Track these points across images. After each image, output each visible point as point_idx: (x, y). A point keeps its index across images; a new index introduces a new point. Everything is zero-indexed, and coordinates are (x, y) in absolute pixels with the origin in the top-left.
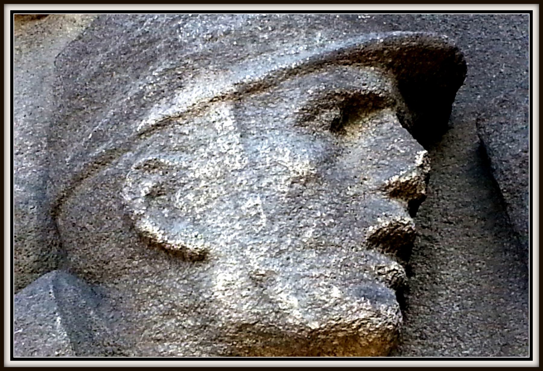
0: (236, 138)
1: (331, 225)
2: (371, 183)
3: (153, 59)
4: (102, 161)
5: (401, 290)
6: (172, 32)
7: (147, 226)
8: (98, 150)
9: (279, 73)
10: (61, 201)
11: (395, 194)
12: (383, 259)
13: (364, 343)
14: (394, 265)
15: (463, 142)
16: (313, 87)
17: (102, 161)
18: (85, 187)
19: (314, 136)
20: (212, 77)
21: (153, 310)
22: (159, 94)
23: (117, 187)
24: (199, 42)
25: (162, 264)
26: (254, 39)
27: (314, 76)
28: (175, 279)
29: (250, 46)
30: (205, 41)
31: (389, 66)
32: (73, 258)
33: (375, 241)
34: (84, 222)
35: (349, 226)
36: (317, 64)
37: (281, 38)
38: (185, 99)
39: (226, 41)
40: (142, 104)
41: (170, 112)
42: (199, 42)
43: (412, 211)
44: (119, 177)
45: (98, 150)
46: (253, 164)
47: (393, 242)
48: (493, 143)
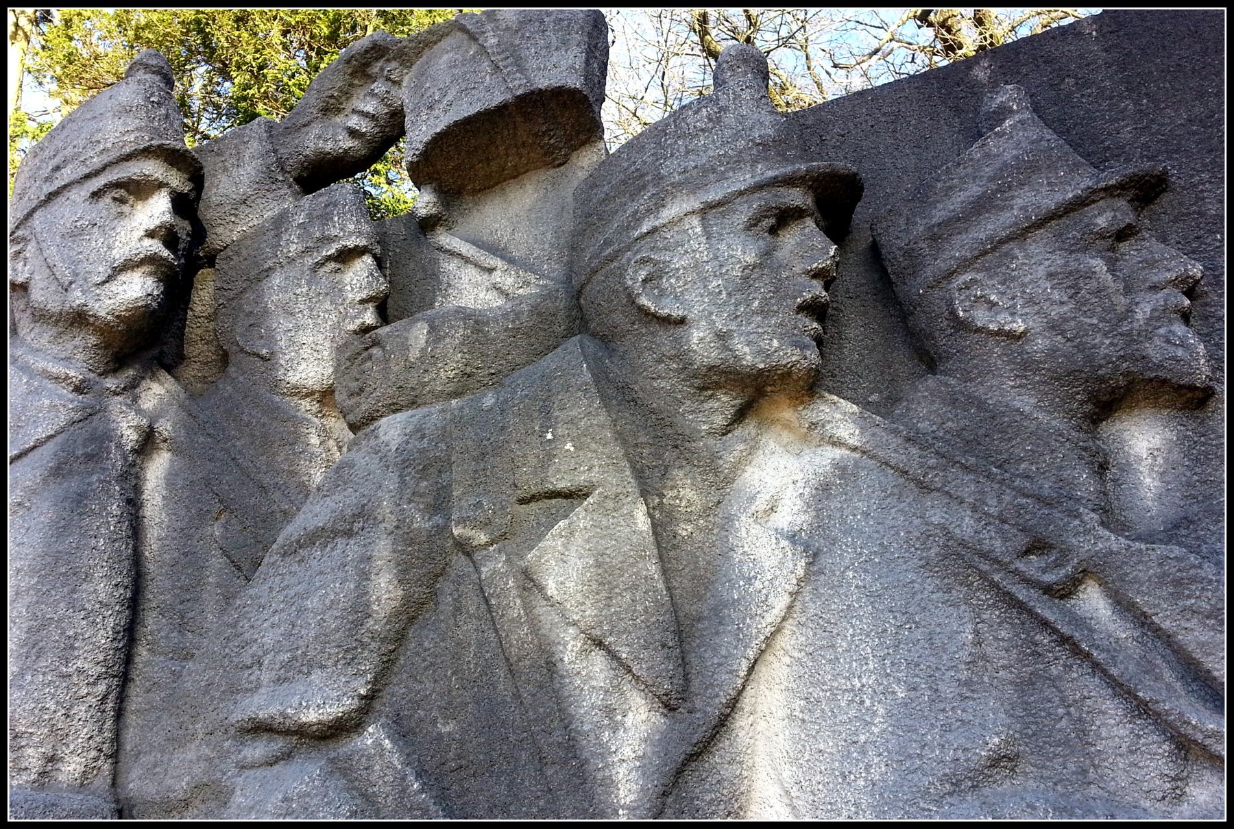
0: (704, 240)
1: (771, 298)
2: (798, 269)
3: (644, 187)
4: (610, 259)
5: (819, 342)
6: (657, 169)
7: (644, 301)
8: (608, 252)
9: (733, 194)
10: (582, 286)
11: (815, 276)
12: (807, 321)
13: (795, 377)
14: (815, 325)
15: (861, 239)
16: (756, 203)
17: (610, 259)
18: (600, 277)
19: (758, 237)
20: (685, 198)
21: (649, 358)
22: (649, 211)
23: (622, 276)
24: (675, 175)
25: (655, 327)
26: (714, 170)
27: (757, 195)
28: (664, 338)
29: (711, 176)
30: (680, 174)
31: (810, 187)
32: (593, 325)
33: (801, 308)
34: (599, 300)
35: (783, 298)
36: (759, 187)
37: (733, 170)
38: (668, 213)
39: (694, 173)
40: (637, 219)
41: (657, 223)
42: (675, 175)
43: (826, 288)
44: (623, 269)
45: (608, 252)
46: (716, 257)
47: (814, 309)
48: (883, 240)
